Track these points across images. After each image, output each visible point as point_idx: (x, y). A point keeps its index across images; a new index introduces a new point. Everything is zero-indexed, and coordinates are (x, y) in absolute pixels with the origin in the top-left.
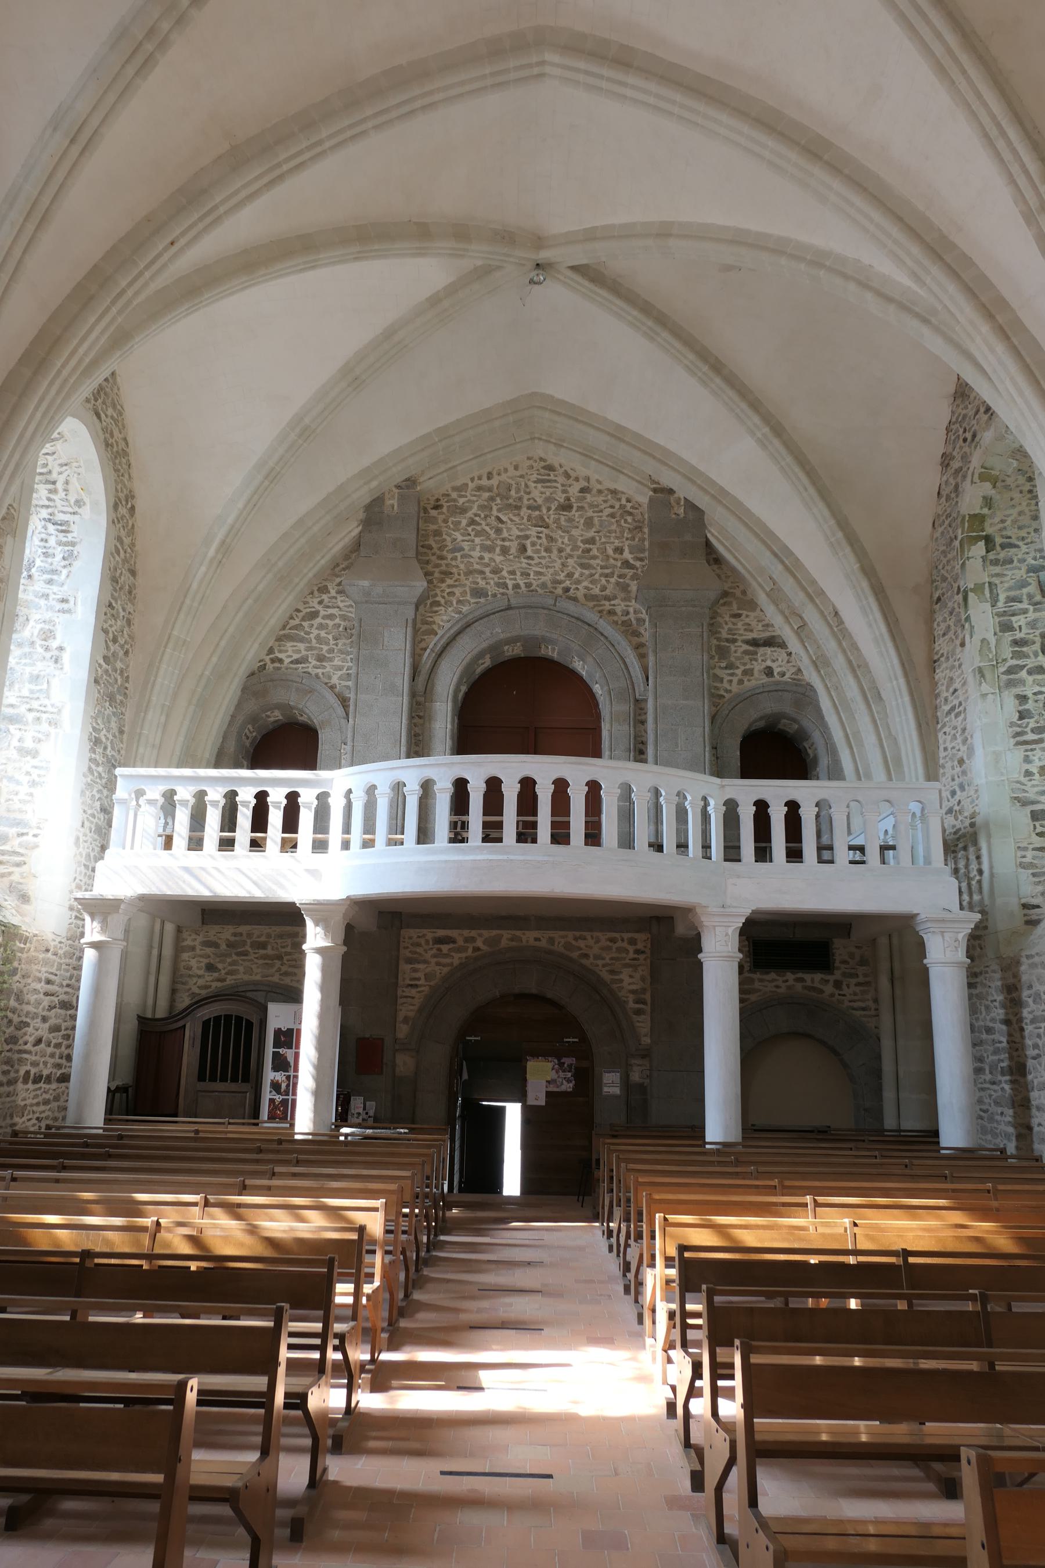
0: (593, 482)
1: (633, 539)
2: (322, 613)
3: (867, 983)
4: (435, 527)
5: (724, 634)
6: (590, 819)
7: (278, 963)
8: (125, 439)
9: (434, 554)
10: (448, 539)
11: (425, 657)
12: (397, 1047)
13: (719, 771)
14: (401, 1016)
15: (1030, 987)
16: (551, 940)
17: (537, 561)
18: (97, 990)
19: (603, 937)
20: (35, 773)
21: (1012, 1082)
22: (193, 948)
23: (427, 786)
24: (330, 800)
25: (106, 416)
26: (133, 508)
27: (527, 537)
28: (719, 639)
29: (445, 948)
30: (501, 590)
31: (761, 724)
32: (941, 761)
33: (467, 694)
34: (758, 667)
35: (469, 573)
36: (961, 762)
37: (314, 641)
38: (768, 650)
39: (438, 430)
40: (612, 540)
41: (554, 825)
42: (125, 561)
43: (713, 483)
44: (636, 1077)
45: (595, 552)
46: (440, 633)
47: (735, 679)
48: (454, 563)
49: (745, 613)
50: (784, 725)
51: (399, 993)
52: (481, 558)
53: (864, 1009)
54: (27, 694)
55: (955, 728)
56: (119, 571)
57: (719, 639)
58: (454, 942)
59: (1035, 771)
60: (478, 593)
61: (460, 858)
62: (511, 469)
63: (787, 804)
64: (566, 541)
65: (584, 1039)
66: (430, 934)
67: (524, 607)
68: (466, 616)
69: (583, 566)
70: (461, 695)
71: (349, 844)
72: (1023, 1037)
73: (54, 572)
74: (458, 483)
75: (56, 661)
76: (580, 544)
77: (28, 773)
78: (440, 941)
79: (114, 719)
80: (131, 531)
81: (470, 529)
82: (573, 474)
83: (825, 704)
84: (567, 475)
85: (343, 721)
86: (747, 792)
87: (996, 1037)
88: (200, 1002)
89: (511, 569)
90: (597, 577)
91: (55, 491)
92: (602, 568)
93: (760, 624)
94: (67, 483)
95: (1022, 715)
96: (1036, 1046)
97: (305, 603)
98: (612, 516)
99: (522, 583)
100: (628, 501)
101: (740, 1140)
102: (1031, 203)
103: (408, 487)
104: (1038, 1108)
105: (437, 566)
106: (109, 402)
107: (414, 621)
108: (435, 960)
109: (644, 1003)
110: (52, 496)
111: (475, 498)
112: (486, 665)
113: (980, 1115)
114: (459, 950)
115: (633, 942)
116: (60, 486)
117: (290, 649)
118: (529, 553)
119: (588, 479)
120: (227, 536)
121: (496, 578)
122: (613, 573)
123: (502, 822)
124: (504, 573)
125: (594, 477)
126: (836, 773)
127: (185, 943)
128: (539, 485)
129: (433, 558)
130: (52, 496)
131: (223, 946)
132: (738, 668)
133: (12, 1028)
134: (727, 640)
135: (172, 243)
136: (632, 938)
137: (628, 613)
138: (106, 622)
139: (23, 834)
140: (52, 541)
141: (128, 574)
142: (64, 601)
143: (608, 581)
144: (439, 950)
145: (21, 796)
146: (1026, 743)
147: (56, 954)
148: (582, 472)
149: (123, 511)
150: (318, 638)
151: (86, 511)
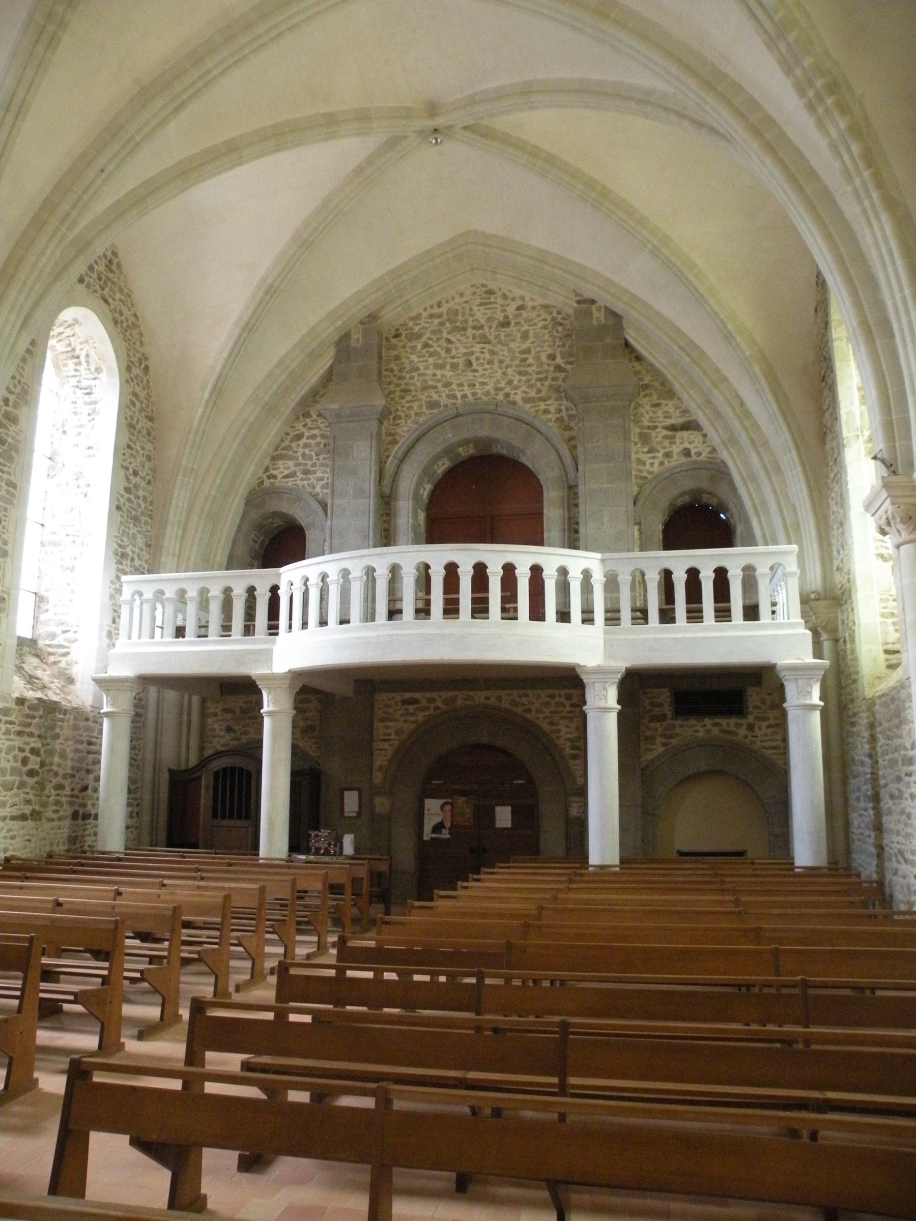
0: (527, 299)
1: (563, 345)
2: (306, 434)
3: (777, 725)
4: (396, 353)
5: (646, 423)
6: (477, 595)
8: (135, 315)
9: (395, 376)
10: (407, 361)
11: (388, 464)
15: (881, 724)
16: (499, 698)
18: (112, 749)
19: (543, 694)
22: (216, 715)
23: (395, 570)
24: (279, 592)
25: (114, 300)
26: (147, 369)
27: (472, 353)
28: (642, 427)
29: (411, 708)
30: (452, 401)
31: (687, 499)
33: (433, 493)
34: (676, 449)
35: (424, 388)
37: (300, 458)
38: (685, 434)
39: (390, 273)
40: (546, 348)
41: (474, 601)
42: (142, 410)
43: (625, 291)
45: (530, 361)
47: (657, 462)
48: (411, 381)
49: (664, 402)
50: (705, 498)
51: (375, 746)
52: (434, 375)
53: (774, 748)
56: (136, 419)
57: (642, 427)
60: (433, 405)
64: (506, 353)
65: (531, 781)
66: (398, 697)
67: (470, 413)
68: (421, 425)
69: (521, 373)
75: (86, 495)
76: (517, 355)
77: (68, 584)
78: (405, 702)
79: (139, 536)
80: (147, 387)
81: (424, 351)
82: (510, 295)
86: (680, 561)
88: (218, 754)
89: (459, 382)
90: (533, 382)
91: (80, 363)
92: (537, 373)
93: (678, 411)
94: (87, 356)
97: (293, 427)
99: (469, 393)
101: (617, 863)
102: (770, 31)
103: (369, 322)
105: (398, 385)
106: (116, 289)
107: (379, 434)
108: (403, 718)
110: (78, 368)
111: (427, 325)
114: (424, 709)
116: (82, 359)
117: (282, 467)
118: (475, 366)
119: (522, 298)
120: (217, 382)
121: (447, 390)
122: (546, 378)
123: (488, 598)
124: (454, 386)
125: (528, 296)
126: (750, 541)
127: (209, 711)
128: (482, 308)
129: (394, 379)
130: (78, 368)
131: (238, 712)
132: (658, 451)
134: (649, 427)
135: (102, 171)
136: (567, 694)
137: (560, 411)
138: (124, 460)
139: (66, 632)
141: (145, 420)
143: (542, 385)
148: (518, 292)
150: (304, 455)
151: (103, 376)
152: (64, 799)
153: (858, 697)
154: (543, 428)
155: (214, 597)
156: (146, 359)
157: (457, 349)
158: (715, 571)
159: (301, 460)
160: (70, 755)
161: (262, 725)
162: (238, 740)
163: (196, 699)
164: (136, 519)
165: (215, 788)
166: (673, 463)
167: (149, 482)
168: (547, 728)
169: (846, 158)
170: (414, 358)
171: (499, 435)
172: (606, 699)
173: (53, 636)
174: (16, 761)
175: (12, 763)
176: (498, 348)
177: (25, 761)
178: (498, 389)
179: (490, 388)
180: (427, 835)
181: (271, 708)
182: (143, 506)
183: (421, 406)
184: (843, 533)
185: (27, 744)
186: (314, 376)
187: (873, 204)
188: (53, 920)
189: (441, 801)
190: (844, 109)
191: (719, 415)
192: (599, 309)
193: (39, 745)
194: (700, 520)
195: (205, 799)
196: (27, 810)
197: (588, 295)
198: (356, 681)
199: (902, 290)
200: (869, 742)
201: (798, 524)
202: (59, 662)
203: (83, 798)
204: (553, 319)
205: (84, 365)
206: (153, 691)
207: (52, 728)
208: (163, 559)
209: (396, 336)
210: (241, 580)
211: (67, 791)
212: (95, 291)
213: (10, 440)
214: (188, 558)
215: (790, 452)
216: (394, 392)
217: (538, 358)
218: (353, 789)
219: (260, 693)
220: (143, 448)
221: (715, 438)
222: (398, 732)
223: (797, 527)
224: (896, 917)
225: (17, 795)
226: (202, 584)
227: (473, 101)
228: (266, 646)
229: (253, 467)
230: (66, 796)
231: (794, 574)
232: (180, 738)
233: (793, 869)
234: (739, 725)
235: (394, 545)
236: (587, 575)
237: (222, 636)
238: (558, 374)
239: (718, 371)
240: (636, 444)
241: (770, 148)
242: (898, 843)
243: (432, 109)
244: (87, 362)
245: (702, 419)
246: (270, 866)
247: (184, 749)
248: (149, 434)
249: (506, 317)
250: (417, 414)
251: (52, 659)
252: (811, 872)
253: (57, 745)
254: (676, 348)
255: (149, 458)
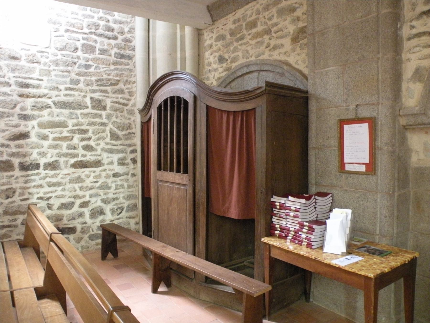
7: (266, 37)
12: (403, 121)
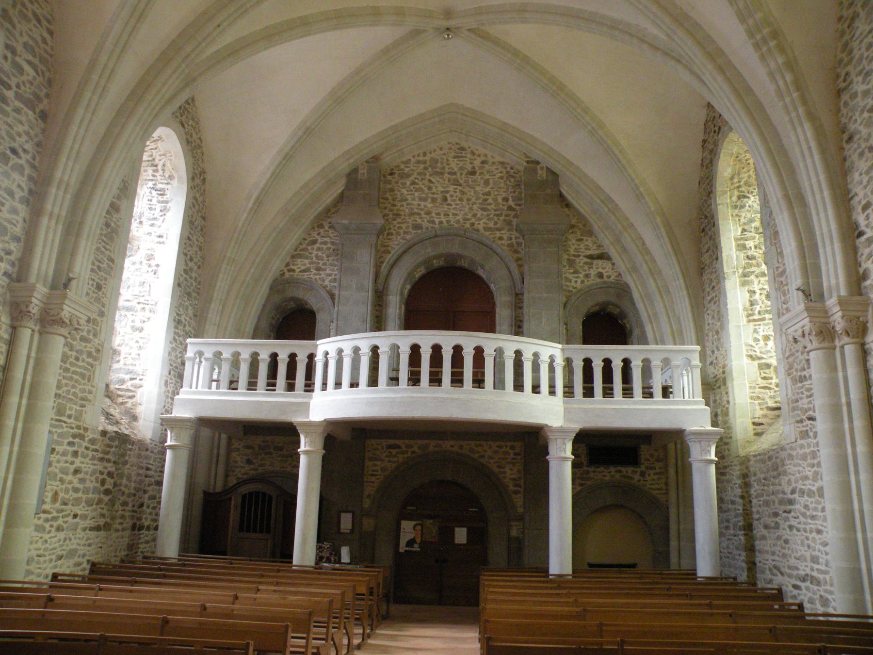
1: (514, 192)
2: (320, 240)
4: (389, 186)
5: (572, 252)
6: (433, 369)
8: (200, 139)
13: (568, 340)
14: (366, 493)
15: (755, 475)
16: (461, 447)
17: (454, 206)
18: (173, 475)
20: (141, 341)
21: (745, 535)
22: (238, 450)
26: (204, 180)
27: (447, 192)
28: (568, 255)
29: (394, 452)
31: (597, 308)
32: (706, 332)
33: (411, 291)
34: (593, 272)
35: (412, 214)
36: (717, 332)
38: (600, 262)
41: (453, 374)
44: (514, 533)
45: (490, 201)
46: (393, 252)
47: (579, 281)
49: (585, 238)
50: (611, 309)
53: (658, 489)
54: (137, 293)
55: (714, 311)
58: (400, 447)
59: (760, 338)
60: (417, 227)
61: (393, 396)
62: (438, 150)
63: (604, 361)
64: (472, 194)
66: (385, 442)
69: (483, 209)
70: (406, 292)
71: (345, 384)
72: (751, 507)
73: (155, 219)
74: (405, 159)
75: (155, 273)
77: (137, 342)
78: (390, 447)
79: (190, 308)
80: (203, 194)
82: (477, 152)
83: (636, 295)
84: (473, 153)
85: (331, 308)
87: (737, 506)
91: (157, 171)
92: (495, 210)
94: (164, 165)
95: (752, 304)
96: (758, 512)
98: (502, 178)
99: (444, 220)
100: (512, 168)
101: (571, 573)
103: (373, 162)
104: (760, 552)
105: (391, 210)
106: (190, 117)
107: (376, 245)
109: (520, 487)
112: (422, 272)
113: (722, 556)
114: (403, 453)
115: (512, 448)
116: (160, 167)
118: (449, 201)
119: (486, 155)
120: (259, 195)
121: (428, 217)
124: (433, 215)
125: (490, 154)
126: (643, 340)
133: (125, 497)
134: (574, 255)
137: (511, 239)
138: (185, 248)
140: (154, 201)
142: (160, 236)
144: (390, 452)
145: (133, 355)
146: (754, 320)
147: (152, 452)
148: (482, 151)
149: (198, 181)
150: (317, 256)
151: (175, 182)
152: (127, 514)
153: (729, 455)
154: (499, 250)
155: (263, 360)
156: (204, 172)
157: (436, 187)
158: (642, 361)
159: (314, 259)
160: (134, 478)
161: (299, 462)
162: (256, 470)
163: (224, 437)
164: (189, 294)
165: (243, 507)
166: (591, 282)
167: (199, 267)
168: (496, 470)
169: (781, 83)
170: (404, 191)
171: (465, 253)
172: (565, 451)
173: (123, 382)
174: (97, 482)
175: (94, 484)
176: (466, 190)
177: (103, 482)
178: (466, 220)
179: (460, 217)
180: (402, 548)
181: (307, 448)
182: (194, 284)
183: (407, 227)
184: (719, 339)
185: (106, 468)
186: (329, 198)
187: (798, 116)
188: (201, 623)
189: (414, 523)
190: (782, 50)
191: (625, 250)
192: (542, 169)
193: (113, 469)
194: (607, 324)
195: (234, 516)
196: (101, 522)
197: (534, 157)
198: (353, 429)
199: (817, 176)
200: (740, 487)
201: (682, 330)
202: (126, 403)
203: (140, 513)
204: (507, 172)
205: (161, 172)
206: (206, 432)
207: (123, 455)
208: (207, 327)
209: (391, 174)
210: (266, 347)
211: (130, 508)
212: (177, 117)
213: (113, 225)
214: (226, 328)
215: (678, 279)
216: (388, 215)
217: (495, 200)
218: (350, 512)
219: (299, 436)
220: (198, 241)
221: (622, 266)
222: (383, 469)
223: (681, 333)
224: (808, 618)
225: (95, 510)
226: (253, 350)
227: (478, 12)
228: (305, 400)
229: (278, 262)
230: (129, 511)
231: (697, 366)
232: (210, 469)
233: (696, 579)
234: (634, 472)
235: (385, 330)
236: (552, 359)
237: (249, 389)
238: (510, 212)
239: (627, 219)
240: (565, 266)
241: (721, 70)
242: (773, 560)
243: (448, 13)
244: (163, 170)
245: (613, 252)
246: (303, 571)
247: (213, 478)
248: (202, 230)
249: (474, 168)
250: (405, 233)
251: (120, 400)
252: (710, 581)
253: (126, 470)
254: (598, 201)
255: (201, 249)
